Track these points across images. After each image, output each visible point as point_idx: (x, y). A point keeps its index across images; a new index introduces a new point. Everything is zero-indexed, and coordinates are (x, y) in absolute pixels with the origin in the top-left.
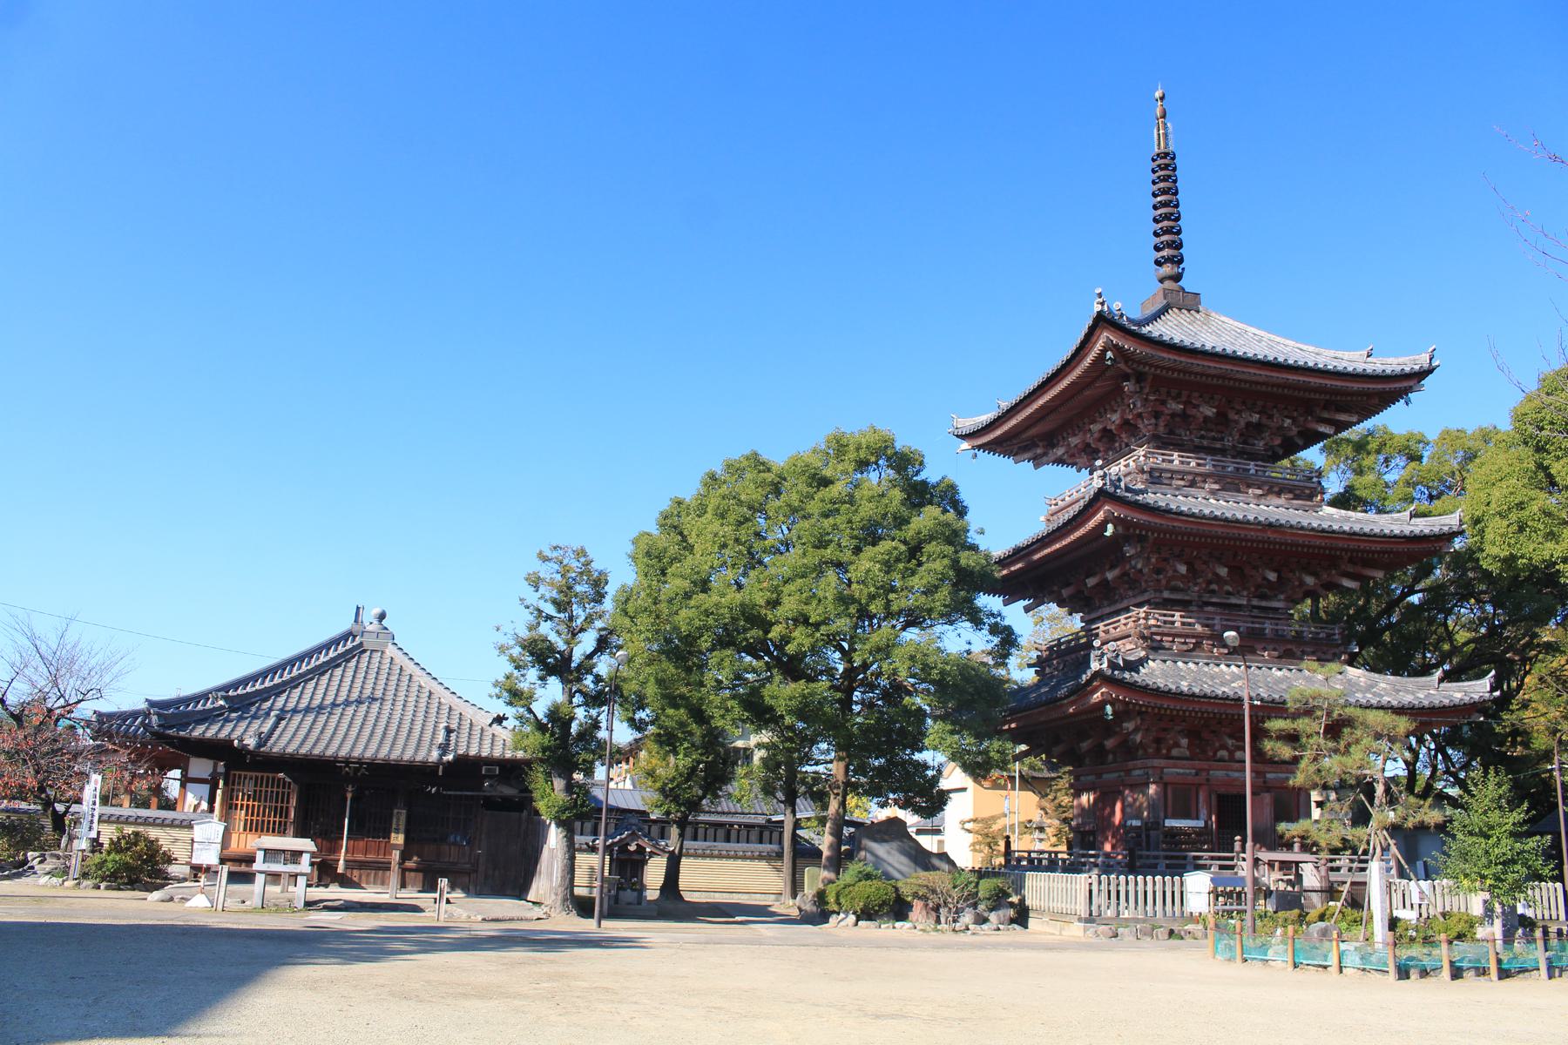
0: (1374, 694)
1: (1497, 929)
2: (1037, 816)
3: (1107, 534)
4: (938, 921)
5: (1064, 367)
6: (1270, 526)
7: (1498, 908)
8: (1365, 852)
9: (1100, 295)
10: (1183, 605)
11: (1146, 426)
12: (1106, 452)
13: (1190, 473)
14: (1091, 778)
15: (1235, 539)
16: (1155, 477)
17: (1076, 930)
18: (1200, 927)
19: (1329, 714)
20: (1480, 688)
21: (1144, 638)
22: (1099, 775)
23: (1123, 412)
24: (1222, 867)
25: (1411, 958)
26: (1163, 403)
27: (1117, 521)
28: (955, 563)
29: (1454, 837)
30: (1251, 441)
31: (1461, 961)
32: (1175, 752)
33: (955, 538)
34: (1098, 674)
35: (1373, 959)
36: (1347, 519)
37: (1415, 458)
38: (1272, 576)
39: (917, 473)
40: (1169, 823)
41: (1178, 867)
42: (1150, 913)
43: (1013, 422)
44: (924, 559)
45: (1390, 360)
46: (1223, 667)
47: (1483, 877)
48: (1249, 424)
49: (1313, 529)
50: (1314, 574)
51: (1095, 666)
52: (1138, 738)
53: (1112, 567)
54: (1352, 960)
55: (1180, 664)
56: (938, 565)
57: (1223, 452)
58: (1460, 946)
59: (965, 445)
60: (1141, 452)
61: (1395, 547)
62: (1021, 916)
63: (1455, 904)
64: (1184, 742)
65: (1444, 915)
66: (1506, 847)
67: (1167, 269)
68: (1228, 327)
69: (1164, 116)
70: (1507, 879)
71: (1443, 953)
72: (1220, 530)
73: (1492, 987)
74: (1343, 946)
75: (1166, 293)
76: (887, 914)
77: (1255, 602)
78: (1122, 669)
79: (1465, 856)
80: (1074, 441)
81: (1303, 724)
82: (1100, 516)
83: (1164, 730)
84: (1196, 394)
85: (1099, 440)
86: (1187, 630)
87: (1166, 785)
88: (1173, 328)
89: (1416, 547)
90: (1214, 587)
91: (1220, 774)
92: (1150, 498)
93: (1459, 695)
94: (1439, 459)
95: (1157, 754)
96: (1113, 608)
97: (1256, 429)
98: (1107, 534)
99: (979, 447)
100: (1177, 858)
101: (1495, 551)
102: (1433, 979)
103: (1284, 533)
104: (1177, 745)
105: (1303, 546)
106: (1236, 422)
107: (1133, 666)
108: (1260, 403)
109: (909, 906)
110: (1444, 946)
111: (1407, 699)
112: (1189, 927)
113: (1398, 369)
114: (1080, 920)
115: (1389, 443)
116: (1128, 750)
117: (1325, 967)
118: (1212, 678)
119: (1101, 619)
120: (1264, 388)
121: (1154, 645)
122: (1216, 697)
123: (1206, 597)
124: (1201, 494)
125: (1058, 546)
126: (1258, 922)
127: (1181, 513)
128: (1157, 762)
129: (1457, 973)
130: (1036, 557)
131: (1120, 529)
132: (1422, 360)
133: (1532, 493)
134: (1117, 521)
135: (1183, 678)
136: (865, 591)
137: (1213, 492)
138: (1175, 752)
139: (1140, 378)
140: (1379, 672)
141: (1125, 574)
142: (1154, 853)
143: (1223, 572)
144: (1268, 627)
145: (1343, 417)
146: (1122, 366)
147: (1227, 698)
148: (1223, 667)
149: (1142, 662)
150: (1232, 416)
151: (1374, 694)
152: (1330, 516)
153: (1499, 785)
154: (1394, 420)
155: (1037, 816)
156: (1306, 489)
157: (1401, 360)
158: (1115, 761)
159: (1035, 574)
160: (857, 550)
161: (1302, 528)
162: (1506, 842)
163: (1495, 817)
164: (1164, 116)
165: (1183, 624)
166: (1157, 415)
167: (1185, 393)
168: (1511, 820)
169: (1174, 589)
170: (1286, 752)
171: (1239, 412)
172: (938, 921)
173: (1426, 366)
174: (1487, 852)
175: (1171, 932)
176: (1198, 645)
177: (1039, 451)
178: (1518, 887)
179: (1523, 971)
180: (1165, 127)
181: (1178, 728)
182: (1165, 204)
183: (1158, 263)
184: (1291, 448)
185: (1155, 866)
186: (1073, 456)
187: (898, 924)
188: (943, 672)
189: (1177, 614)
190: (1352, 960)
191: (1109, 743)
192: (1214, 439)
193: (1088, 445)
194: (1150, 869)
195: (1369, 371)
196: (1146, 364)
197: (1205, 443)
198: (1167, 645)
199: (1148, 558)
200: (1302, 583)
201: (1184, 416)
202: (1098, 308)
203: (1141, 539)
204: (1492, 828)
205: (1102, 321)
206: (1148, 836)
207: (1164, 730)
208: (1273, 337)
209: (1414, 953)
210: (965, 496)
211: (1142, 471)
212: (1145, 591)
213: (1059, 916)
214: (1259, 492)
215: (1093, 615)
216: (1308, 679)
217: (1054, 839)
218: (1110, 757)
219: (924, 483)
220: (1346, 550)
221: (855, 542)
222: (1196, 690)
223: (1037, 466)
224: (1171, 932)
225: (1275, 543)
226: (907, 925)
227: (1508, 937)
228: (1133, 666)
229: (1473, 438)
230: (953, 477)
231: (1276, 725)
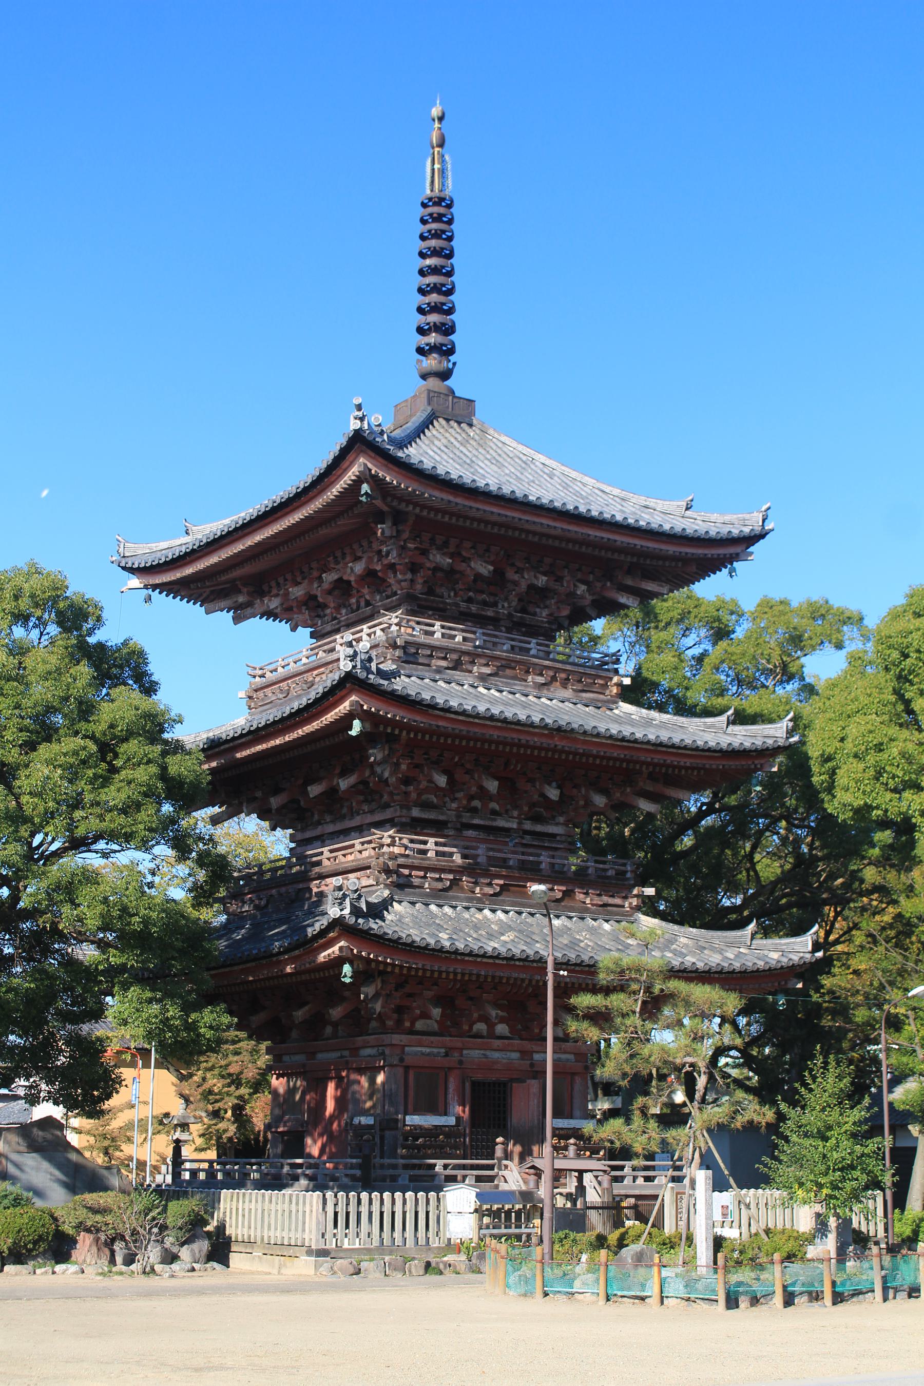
0: (675, 952)
1: (830, 1244)
2: (177, 1108)
3: (354, 732)
4: (112, 1261)
5: (298, 495)
6: (559, 731)
7: (832, 1222)
8: (680, 1159)
9: (359, 407)
10: (437, 827)
11: (398, 582)
12: (338, 609)
13: (454, 651)
14: (300, 1058)
15: (512, 745)
16: (411, 654)
17: (304, 1266)
18: (463, 1257)
19: (648, 990)
20: (799, 948)
21: (387, 871)
22: (312, 1055)
23: (370, 559)
24: (479, 1179)
25: (740, 1284)
26: (424, 552)
27: (366, 716)
28: (163, 775)
29: (787, 1140)
30: (531, 609)
31: (794, 1284)
32: (420, 1025)
33: (153, 727)
34: (337, 923)
35: (700, 1286)
36: (649, 722)
37: (721, 633)
38: (553, 794)
39: (91, 632)
40: (413, 1120)
41: (429, 1183)
42: (398, 1241)
43: (213, 559)
44: (118, 763)
45: (714, 517)
46: (487, 912)
47: (820, 1186)
48: (531, 587)
49: (611, 737)
50: (605, 792)
51: (334, 912)
52: (378, 1007)
53: (344, 773)
54: (676, 1288)
55: (433, 907)
56: (143, 774)
57: (494, 622)
58: (795, 1267)
59: (135, 582)
60: (393, 618)
61: (708, 764)
62: (220, 1250)
63: (777, 1219)
64: (436, 1012)
65: (767, 1231)
66: (843, 1149)
67: (432, 362)
68: (509, 456)
69: (441, 145)
70: (840, 1185)
71: (775, 1276)
72: (495, 734)
73: (826, 1311)
74: (665, 1273)
75: (431, 396)
76: (44, 1253)
77: (528, 826)
78: (365, 916)
79: (798, 1160)
80: (297, 592)
81: (617, 1001)
82: (345, 707)
83: (410, 995)
84: (467, 544)
85: (329, 592)
86: (443, 862)
87: (407, 1068)
88: (439, 452)
89: (733, 764)
90: (476, 803)
91: (476, 1054)
92: (400, 684)
93: (775, 956)
94: (755, 638)
95: (398, 1028)
96: (339, 826)
97: (539, 595)
98: (354, 732)
99: (154, 587)
100: (420, 1167)
101: (847, 798)
102: (764, 1307)
103: (575, 740)
104: (426, 1015)
105: (595, 757)
106: (516, 583)
107: (377, 911)
108: (548, 560)
109: (72, 1242)
110: (777, 1268)
111: (714, 960)
112: (449, 1258)
113: (724, 531)
114: (310, 1252)
115: (695, 612)
116: (358, 1021)
117: (643, 1299)
118: (476, 928)
119: (322, 840)
120: (557, 543)
121: (401, 881)
122: (484, 956)
123: (466, 818)
124: (468, 679)
125: (278, 742)
126: (557, 1247)
127: (449, 710)
128: (397, 1039)
129: (789, 1301)
130: (238, 755)
131: (368, 725)
132: (751, 522)
133: (893, 731)
134: (366, 716)
135: (440, 928)
136: (41, 809)
137: (483, 678)
138: (420, 1025)
139: (398, 518)
140: (681, 923)
141: (365, 783)
142: (381, 1161)
143: (492, 786)
144: (545, 859)
145: (651, 586)
146: (378, 503)
147: (498, 957)
148: (487, 912)
149: (386, 904)
150: (511, 575)
151: (675, 952)
152: (627, 719)
153: (840, 1077)
154: (710, 589)
155: (177, 1108)
156: (590, 676)
157: (727, 518)
158: (335, 1035)
159: (243, 774)
160: (30, 746)
161: (598, 735)
162: (846, 1143)
163: (834, 1116)
164: (441, 145)
165: (438, 853)
166: (414, 568)
167: (453, 542)
168: (851, 1120)
169: (426, 806)
170: (592, 1033)
171: (519, 571)
172: (112, 1261)
173: (758, 529)
174: (824, 1156)
175: (428, 1265)
176: (455, 883)
177: (241, 599)
178: (855, 1196)
179: (857, 1293)
180: (443, 161)
181: (429, 994)
182: (435, 270)
183: (420, 351)
184: (580, 616)
185: (394, 1179)
186: (289, 609)
187: (59, 1268)
188: (146, 921)
189: (432, 840)
190: (676, 1288)
191: (336, 1013)
192: (485, 603)
193: (313, 598)
194: (391, 1184)
195: (689, 531)
196: (408, 502)
197: (474, 608)
198: (416, 882)
199: (397, 765)
200: (588, 803)
201: (451, 574)
202: (355, 425)
203: (391, 739)
204: (830, 1128)
205: (359, 442)
206: (382, 1138)
207: (410, 995)
208: (567, 470)
209: (742, 1274)
210: (156, 669)
211: (394, 646)
212: (386, 806)
213: (281, 1249)
214: (541, 680)
215: (308, 834)
216: (593, 931)
217: (199, 1141)
218: (329, 1030)
220: (648, 764)
221: (24, 736)
222: (460, 946)
223: (237, 620)
224: (428, 1265)
225: (562, 751)
226: (72, 1268)
227: (842, 1256)
228: (377, 911)
229: (797, 612)
230: (142, 640)
231: (584, 1001)
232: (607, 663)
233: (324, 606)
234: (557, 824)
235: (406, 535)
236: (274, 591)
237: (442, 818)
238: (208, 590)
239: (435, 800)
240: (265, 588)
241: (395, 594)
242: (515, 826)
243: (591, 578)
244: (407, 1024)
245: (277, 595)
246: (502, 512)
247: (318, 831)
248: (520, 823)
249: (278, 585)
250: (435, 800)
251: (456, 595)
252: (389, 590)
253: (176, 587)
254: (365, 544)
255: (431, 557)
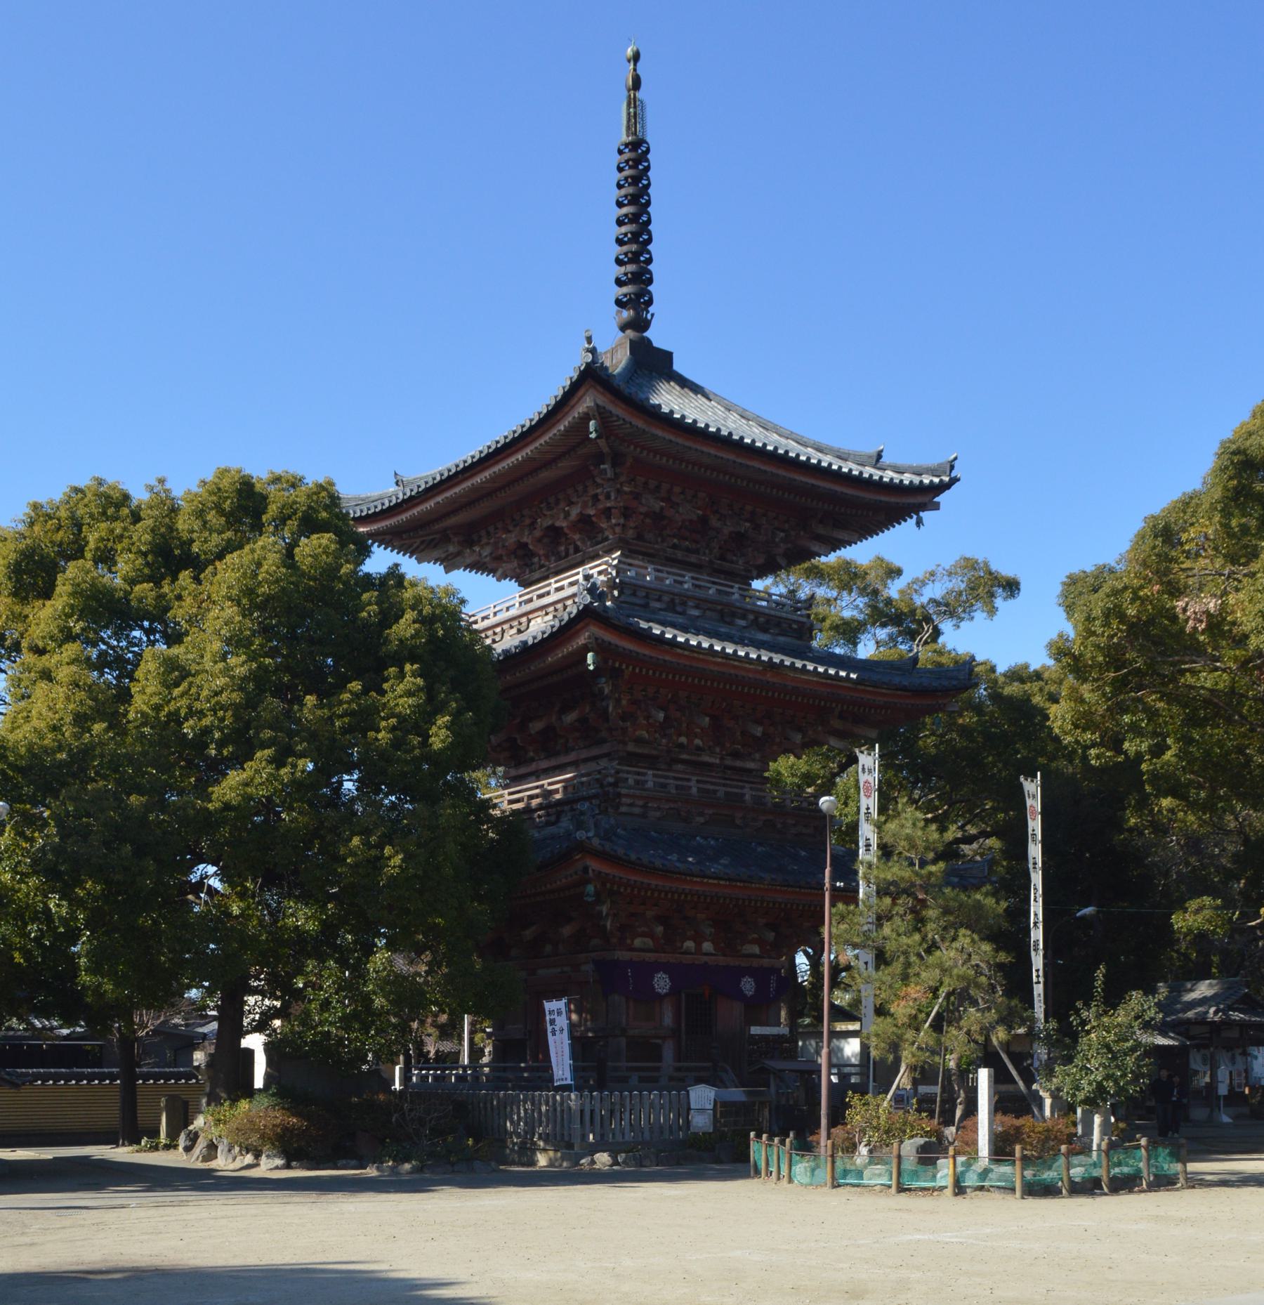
23: (585, 505)
26: (637, 496)
27: (602, 649)
80: (511, 539)
84: (677, 489)
85: (539, 540)
96: (553, 762)
150: (714, 522)
166: (627, 513)
167: (665, 486)
177: (451, 549)
192: (688, 550)
197: (679, 555)
201: (658, 517)
212: (604, 741)
219: (368, 575)
232: (799, 609)
233: (533, 554)
234: (754, 760)
235: (623, 479)
236: (484, 541)
237: (655, 753)
238: (418, 541)
239: (646, 736)
240: (475, 537)
241: (607, 539)
242: (718, 761)
243: (787, 526)
244: (629, 941)
245: (488, 544)
246: (720, 454)
247: (533, 767)
248: (722, 759)
249: (488, 533)
250: (646, 736)
251: (663, 541)
252: (600, 536)
253: (388, 537)
254: (580, 488)
255: (644, 501)
